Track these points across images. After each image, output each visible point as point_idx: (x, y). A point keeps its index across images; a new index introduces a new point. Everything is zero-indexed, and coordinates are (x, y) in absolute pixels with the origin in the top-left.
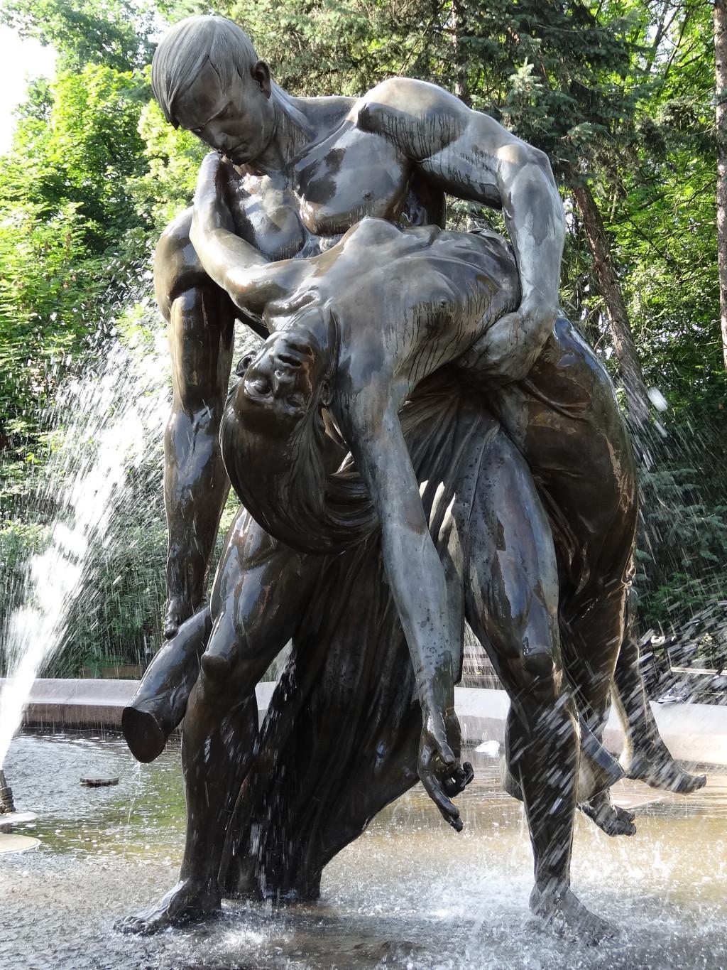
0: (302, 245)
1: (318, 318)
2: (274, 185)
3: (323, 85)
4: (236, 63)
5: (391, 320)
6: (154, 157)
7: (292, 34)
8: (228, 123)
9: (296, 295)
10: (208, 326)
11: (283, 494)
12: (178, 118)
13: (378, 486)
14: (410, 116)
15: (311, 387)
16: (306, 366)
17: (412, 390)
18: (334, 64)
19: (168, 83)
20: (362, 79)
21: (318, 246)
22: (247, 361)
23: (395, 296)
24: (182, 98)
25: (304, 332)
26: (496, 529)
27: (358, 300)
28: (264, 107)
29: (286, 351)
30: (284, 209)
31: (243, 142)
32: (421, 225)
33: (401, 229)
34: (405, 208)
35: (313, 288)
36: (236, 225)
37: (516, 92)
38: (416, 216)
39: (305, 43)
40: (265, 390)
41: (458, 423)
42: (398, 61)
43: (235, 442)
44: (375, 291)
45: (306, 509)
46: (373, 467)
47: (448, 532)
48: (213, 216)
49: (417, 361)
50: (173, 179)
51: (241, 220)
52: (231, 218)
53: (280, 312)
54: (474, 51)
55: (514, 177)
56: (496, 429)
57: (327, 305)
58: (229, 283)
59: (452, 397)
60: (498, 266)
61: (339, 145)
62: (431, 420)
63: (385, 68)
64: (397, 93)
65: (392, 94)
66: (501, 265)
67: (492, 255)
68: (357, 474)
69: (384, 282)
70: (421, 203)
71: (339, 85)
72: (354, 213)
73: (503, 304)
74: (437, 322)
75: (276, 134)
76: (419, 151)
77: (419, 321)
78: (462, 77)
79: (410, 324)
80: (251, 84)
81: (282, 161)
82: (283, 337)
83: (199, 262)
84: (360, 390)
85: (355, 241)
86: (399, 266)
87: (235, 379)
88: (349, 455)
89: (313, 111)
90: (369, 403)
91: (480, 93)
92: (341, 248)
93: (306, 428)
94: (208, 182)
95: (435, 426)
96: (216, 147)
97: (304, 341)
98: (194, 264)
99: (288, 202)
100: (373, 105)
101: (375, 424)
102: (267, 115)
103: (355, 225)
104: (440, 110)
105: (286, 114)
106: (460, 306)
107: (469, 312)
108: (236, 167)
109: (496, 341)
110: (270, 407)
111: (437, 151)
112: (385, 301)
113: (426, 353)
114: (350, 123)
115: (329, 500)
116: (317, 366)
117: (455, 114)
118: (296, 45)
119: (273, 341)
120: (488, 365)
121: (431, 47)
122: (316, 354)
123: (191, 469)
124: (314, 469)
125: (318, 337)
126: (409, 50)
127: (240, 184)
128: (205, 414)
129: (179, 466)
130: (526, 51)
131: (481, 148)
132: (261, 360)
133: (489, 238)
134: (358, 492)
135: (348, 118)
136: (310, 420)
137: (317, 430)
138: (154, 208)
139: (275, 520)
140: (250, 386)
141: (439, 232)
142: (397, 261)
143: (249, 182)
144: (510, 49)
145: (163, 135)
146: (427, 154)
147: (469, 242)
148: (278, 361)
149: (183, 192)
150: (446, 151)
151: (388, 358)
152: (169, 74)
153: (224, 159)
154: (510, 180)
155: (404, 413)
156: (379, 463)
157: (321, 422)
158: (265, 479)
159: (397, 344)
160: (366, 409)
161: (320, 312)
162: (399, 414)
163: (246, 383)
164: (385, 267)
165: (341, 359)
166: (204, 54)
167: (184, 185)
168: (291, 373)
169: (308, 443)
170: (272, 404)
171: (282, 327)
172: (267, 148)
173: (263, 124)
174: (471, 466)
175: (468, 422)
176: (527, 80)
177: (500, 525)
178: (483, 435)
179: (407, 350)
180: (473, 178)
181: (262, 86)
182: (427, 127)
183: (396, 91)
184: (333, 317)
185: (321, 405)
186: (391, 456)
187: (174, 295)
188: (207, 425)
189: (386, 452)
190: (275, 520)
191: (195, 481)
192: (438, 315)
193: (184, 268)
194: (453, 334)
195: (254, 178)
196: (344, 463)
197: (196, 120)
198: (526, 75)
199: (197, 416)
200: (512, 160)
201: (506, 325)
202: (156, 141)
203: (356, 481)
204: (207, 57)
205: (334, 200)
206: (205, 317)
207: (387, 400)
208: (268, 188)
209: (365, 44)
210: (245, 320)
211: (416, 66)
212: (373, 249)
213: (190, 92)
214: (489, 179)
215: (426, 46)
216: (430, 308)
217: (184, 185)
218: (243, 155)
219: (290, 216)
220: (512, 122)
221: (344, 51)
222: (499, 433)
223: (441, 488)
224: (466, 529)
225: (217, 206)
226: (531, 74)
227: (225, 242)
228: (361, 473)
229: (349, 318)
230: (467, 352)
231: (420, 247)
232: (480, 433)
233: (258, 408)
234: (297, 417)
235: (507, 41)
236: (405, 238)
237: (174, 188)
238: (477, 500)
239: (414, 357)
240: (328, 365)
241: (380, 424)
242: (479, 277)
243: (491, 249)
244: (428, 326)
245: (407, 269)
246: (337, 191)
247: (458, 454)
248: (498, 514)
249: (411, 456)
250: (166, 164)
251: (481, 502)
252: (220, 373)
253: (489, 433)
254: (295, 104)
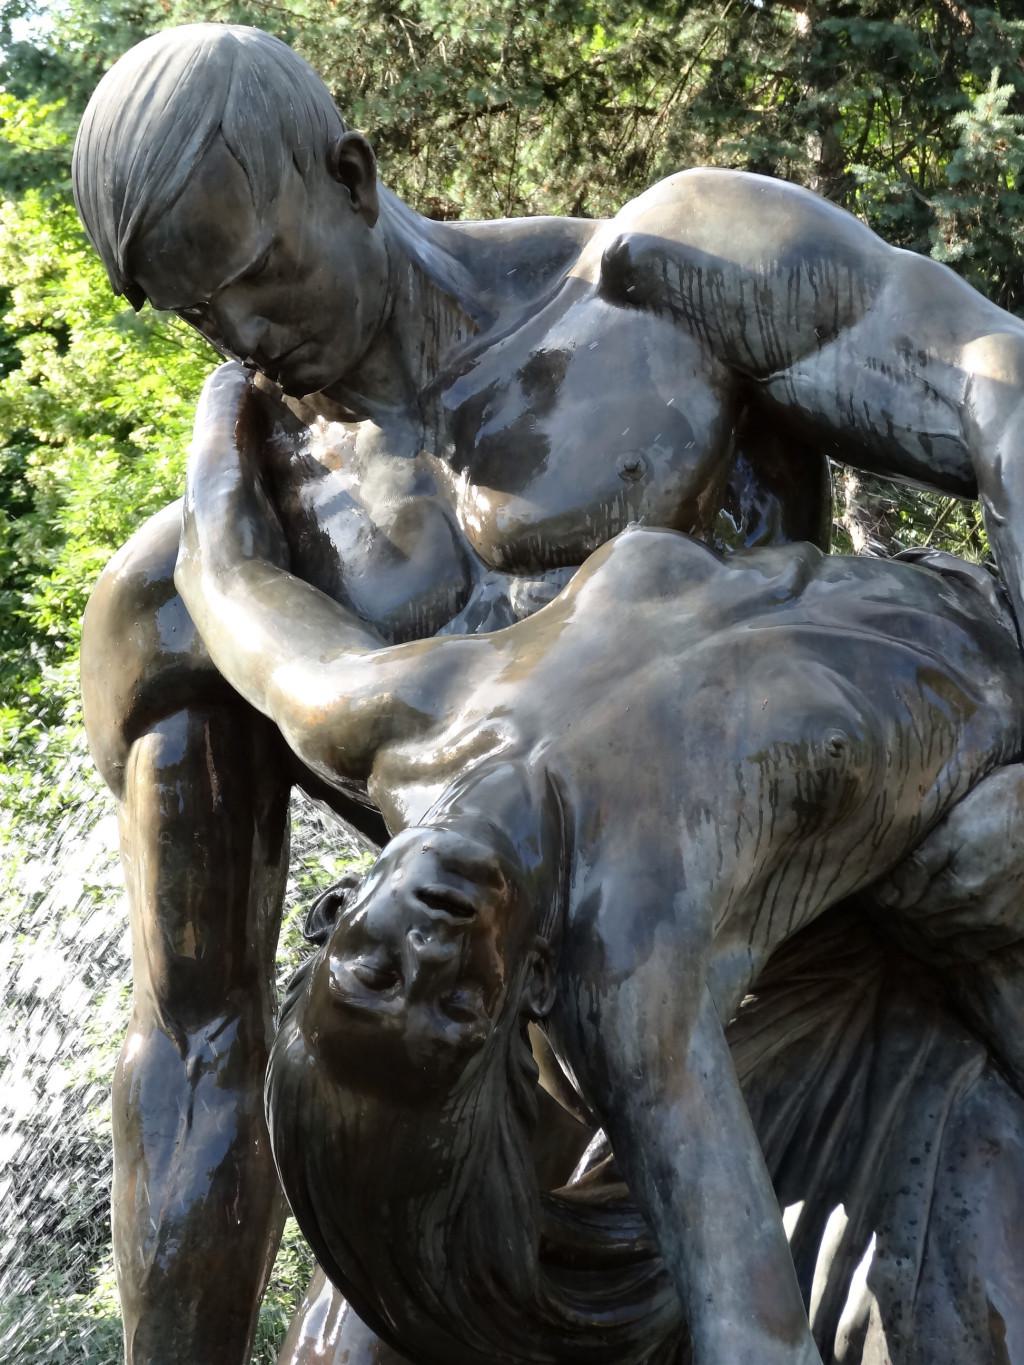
0: (463, 598)
1: (514, 791)
2: (390, 445)
3: (467, 145)
4: (290, 142)
5: (700, 791)
6: (29, 329)
7: (391, 20)
8: (270, 292)
9: (455, 727)
11: (432, 1247)
12: (143, 283)
13: (678, 1222)
14: (735, 267)
15: (501, 970)
16: (487, 912)
17: (758, 968)
18: (499, 94)
19: (118, 194)
20: (569, 127)
22: (334, 904)
23: (712, 732)
24: (154, 233)
25: (483, 828)
26: (984, 1327)
28: (363, 249)
29: (440, 880)
30: (416, 506)
31: (308, 338)
32: (766, 542)
33: (720, 554)
34: (728, 498)
35: (499, 712)
36: (293, 548)
37: (969, 156)
38: (754, 515)
39: (426, 42)
40: (383, 979)
41: (877, 1050)
42: (661, 81)
43: (306, 1114)
44: (661, 719)
45: (490, 1285)
46: (665, 1173)
47: (858, 1335)
48: (233, 528)
49: (771, 893)
50: (83, 384)
51: (304, 535)
52: (278, 528)
53: (410, 775)
54: (857, 55)
55: (1007, 416)
56: (976, 1064)
57: (535, 755)
58: (279, 701)
59: (860, 982)
60: (972, 646)
61: (554, 340)
62: (807, 1043)
63: (627, 98)
64: (702, 206)
65: (688, 210)
66: (981, 646)
67: (956, 616)
68: (622, 1188)
70: (766, 483)
71: (511, 144)
72: (596, 513)
73: (988, 744)
74: (822, 794)
75: (392, 318)
76: (759, 353)
77: (775, 792)
78: (826, 121)
79: (752, 800)
80: (328, 191)
81: (409, 384)
82: (427, 843)
83: (199, 641)
84: (627, 975)
85: (603, 589)
86: (719, 651)
88: (600, 1137)
89: (487, 253)
91: (871, 158)
92: (568, 607)
93: (490, 1073)
94: (218, 440)
95: (817, 1060)
96: (240, 353)
97: (483, 852)
98: (183, 647)
99: (424, 484)
100: (638, 239)
101: (667, 1062)
102: (368, 268)
104: (810, 252)
105: (417, 265)
106: (878, 750)
107: (903, 764)
108: (292, 403)
109: (973, 839)
110: (396, 1022)
111: (806, 351)
112: (687, 742)
113: (794, 874)
114: (581, 284)
115: (550, 1258)
116: (513, 911)
117: (852, 259)
118: (402, 49)
119: (401, 853)
121: (748, 47)
122: (514, 885)
123: (184, 1175)
124: (510, 1180)
125: (517, 839)
126: (689, 54)
127: (302, 444)
128: (210, 1039)
129: (152, 1166)
130: (991, 52)
131: (918, 344)
132: (368, 903)
133: (945, 573)
134: (625, 1235)
135: (574, 273)
136: (500, 1054)
138: (33, 458)
139: (411, 1315)
140: (344, 969)
142: (715, 640)
143: (324, 437)
144: (951, 47)
145: (52, 275)
146: (781, 360)
148: (416, 904)
149: (107, 417)
150: (829, 353)
151: (696, 891)
152: (118, 171)
153: (258, 380)
154: (997, 425)
155: (740, 1028)
156: (681, 1163)
157: (526, 1059)
158: (385, 1210)
160: (642, 1025)
161: (520, 773)
162: (729, 1030)
163: (334, 960)
164: (685, 656)
165: (578, 894)
166: (207, 121)
167: (109, 402)
168: (452, 933)
170: (402, 1016)
171: (422, 809)
172: (371, 349)
173: (359, 293)
174: (915, 1161)
176: (997, 125)
177: (994, 1315)
178: (944, 1080)
179: (744, 868)
180: (900, 421)
181: (354, 197)
182: (779, 290)
183: (698, 203)
184: (553, 786)
185: (527, 1015)
186: (713, 1144)
187: (132, 729)
188: (222, 1064)
189: (696, 1134)
190: (411, 1315)
191: (195, 1209)
192: (825, 775)
193: (158, 658)
195: (337, 427)
196: (585, 1160)
197: (188, 286)
198: (993, 114)
199: (198, 1039)
200: (999, 375)
201: (999, 797)
202: (35, 289)
203: (617, 1207)
204: (217, 128)
205: (542, 481)
208: (373, 452)
209: (576, 38)
210: (317, 790)
211: (709, 93)
213: (173, 218)
214: (943, 422)
215: (734, 44)
217: (109, 402)
218: (308, 371)
219: (431, 524)
220: (963, 234)
221: (525, 58)
222: (985, 1073)
223: (837, 1221)
224: (907, 1326)
225: (244, 502)
226: (1007, 111)
227: (267, 596)
228: (633, 1187)
229: (593, 789)
230: (899, 868)
231: (771, 601)
232: (935, 1075)
234: (467, 1048)
235: (940, 29)
236: (734, 577)
237: (85, 406)
238: (934, 1250)
239: (762, 886)
240: (542, 912)
241: (680, 1060)
242: (924, 675)
243: (954, 603)
244: (797, 804)
245: (740, 657)
246: (552, 461)
247: (880, 1129)
248: (989, 1286)
249: (760, 1134)
250: (63, 347)
251: (943, 1255)
253: (962, 1070)
254: (442, 238)
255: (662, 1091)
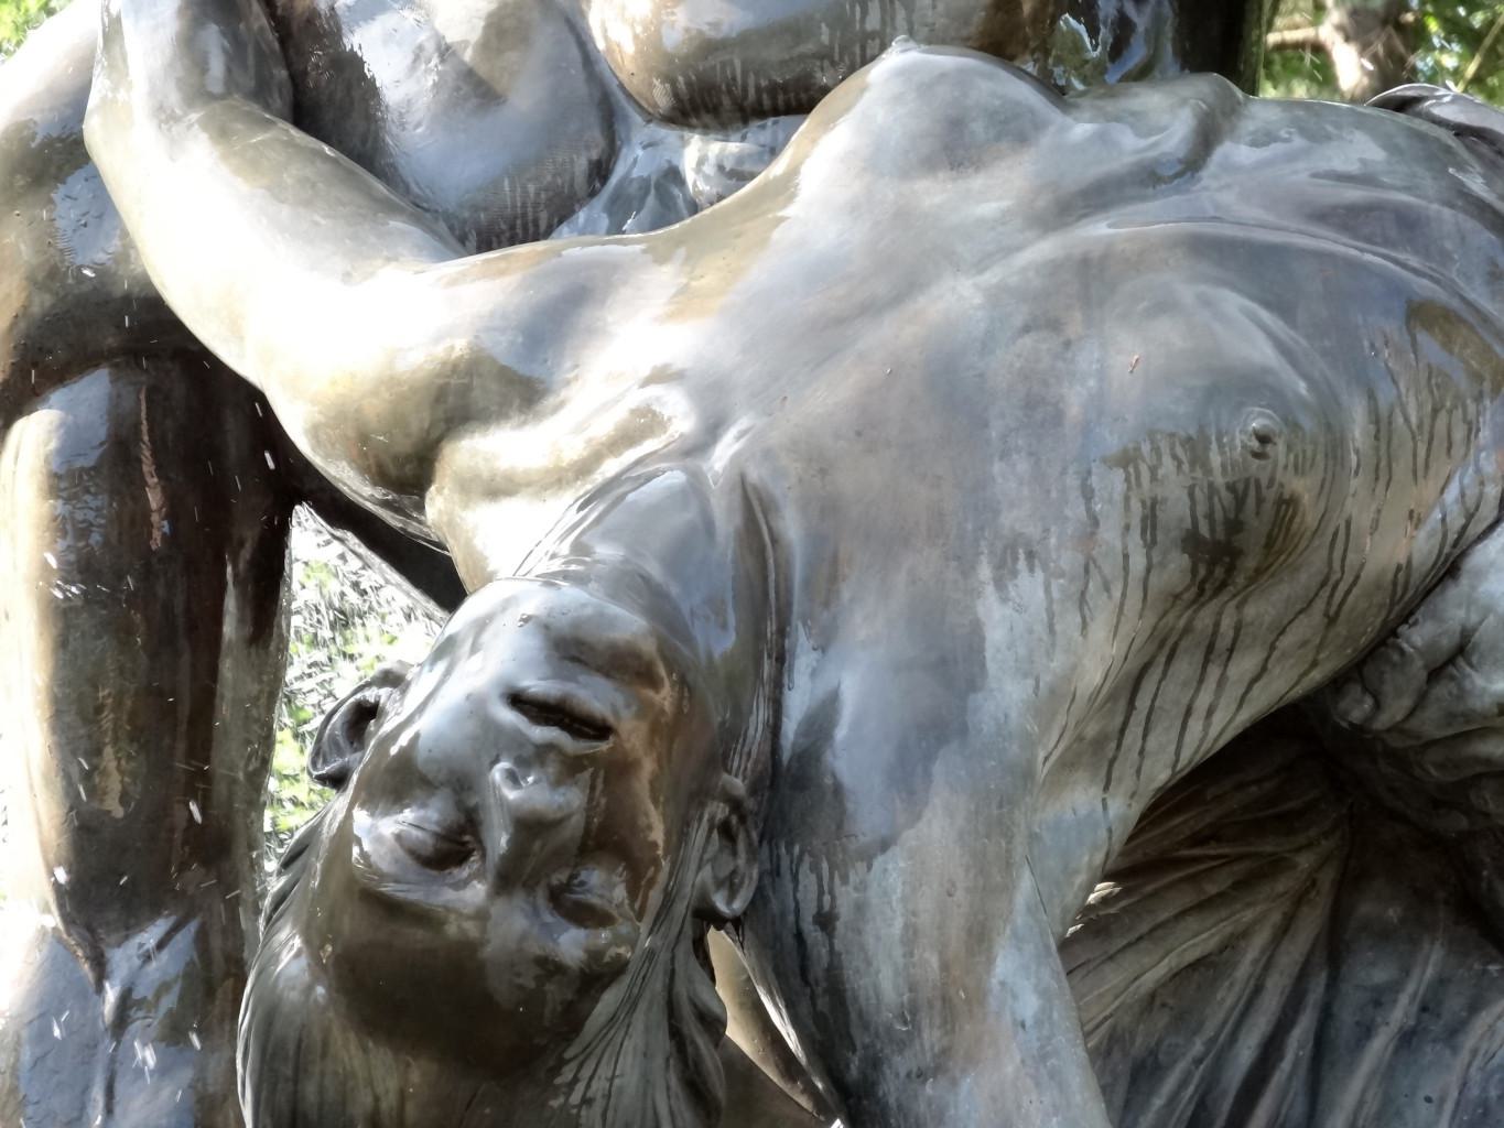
0: (600, 171)
1: (690, 515)
5: (1015, 520)
10: (171, 539)
15: (658, 835)
16: (632, 733)
17: (1121, 834)
21: (674, 175)
22: (364, 715)
27: (866, 428)
33: (1058, 93)
35: (661, 376)
36: (297, 80)
40: (450, 850)
43: (310, 1090)
48: (189, 43)
49: (1143, 702)
51: (317, 57)
55: (1172, 606)
59: (1305, 861)
62: (1208, 968)
69: (987, 344)
74: (1235, 525)
77: (1150, 522)
79: (1110, 534)
84: (885, 845)
86: (1054, 268)
87: (294, 799)
90: (926, 904)
92: (785, 188)
93: (639, 1019)
95: (1227, 997)
97: (629, 624)
101: (955, 1000)
103: (853, 82)
106: (1336, 447)
107: (1381, 472)
110: (472, 929)
113: (1184, 667)
119: (481, 625)
120: (1468, 716)
122: (683, 683)
132: (425, 716)
133: (1461, 131)
137: (689, 1028)
140: (382, 833)
141: (1232, 111)
142: (1046, 248)
147: (1376, 154)
148: (508, 716)
155: (1088, 941)
159: (1047, 635)
160: (911, 935)
161: (695, 487)
163: (361, 818)
164: (992, 277)
165: (798, 702)
168: (572, 767)
169: (646, 1080)
170: (481, 916)
175: (1381, 975)
178: (1453, 1033)
179: (1097, 654)
184: (754, 508)
185: (706, 916)
188: (169, 1001)
193: (50, 276)
194: (1306, 578)
199: (122, 959)
206: (154, 499)
207: (1008, 888)
210: (340, 512)
212: (934, 193)
216: (1198, 458)
227: (251, 165)
229: (826, 510)
230: (1369, 661)
231: (1149, 178)
233: (418, 936)
234: (596, 976)
239: (1130, 686)
240: (732, 734)
241: (978, 997)
242: (1420, 314)
244: (1192, 542)
245: (1091, 278)
252: (229, 756)
255: (946, 1052)
